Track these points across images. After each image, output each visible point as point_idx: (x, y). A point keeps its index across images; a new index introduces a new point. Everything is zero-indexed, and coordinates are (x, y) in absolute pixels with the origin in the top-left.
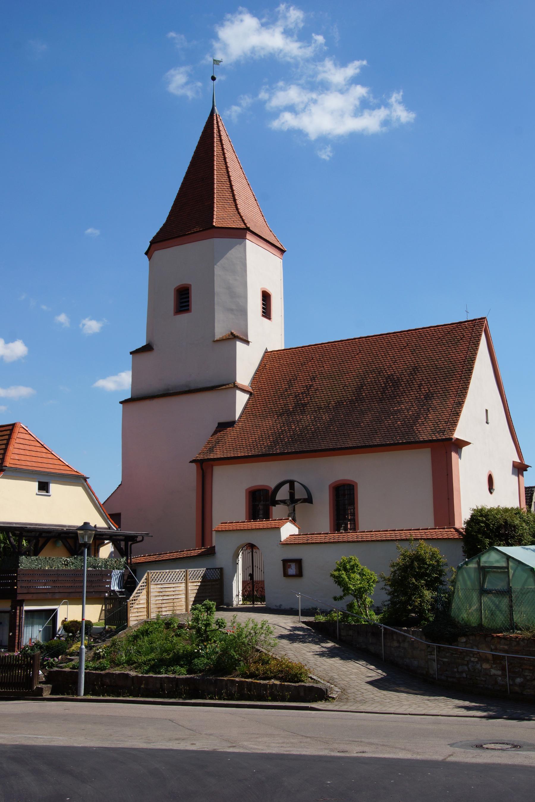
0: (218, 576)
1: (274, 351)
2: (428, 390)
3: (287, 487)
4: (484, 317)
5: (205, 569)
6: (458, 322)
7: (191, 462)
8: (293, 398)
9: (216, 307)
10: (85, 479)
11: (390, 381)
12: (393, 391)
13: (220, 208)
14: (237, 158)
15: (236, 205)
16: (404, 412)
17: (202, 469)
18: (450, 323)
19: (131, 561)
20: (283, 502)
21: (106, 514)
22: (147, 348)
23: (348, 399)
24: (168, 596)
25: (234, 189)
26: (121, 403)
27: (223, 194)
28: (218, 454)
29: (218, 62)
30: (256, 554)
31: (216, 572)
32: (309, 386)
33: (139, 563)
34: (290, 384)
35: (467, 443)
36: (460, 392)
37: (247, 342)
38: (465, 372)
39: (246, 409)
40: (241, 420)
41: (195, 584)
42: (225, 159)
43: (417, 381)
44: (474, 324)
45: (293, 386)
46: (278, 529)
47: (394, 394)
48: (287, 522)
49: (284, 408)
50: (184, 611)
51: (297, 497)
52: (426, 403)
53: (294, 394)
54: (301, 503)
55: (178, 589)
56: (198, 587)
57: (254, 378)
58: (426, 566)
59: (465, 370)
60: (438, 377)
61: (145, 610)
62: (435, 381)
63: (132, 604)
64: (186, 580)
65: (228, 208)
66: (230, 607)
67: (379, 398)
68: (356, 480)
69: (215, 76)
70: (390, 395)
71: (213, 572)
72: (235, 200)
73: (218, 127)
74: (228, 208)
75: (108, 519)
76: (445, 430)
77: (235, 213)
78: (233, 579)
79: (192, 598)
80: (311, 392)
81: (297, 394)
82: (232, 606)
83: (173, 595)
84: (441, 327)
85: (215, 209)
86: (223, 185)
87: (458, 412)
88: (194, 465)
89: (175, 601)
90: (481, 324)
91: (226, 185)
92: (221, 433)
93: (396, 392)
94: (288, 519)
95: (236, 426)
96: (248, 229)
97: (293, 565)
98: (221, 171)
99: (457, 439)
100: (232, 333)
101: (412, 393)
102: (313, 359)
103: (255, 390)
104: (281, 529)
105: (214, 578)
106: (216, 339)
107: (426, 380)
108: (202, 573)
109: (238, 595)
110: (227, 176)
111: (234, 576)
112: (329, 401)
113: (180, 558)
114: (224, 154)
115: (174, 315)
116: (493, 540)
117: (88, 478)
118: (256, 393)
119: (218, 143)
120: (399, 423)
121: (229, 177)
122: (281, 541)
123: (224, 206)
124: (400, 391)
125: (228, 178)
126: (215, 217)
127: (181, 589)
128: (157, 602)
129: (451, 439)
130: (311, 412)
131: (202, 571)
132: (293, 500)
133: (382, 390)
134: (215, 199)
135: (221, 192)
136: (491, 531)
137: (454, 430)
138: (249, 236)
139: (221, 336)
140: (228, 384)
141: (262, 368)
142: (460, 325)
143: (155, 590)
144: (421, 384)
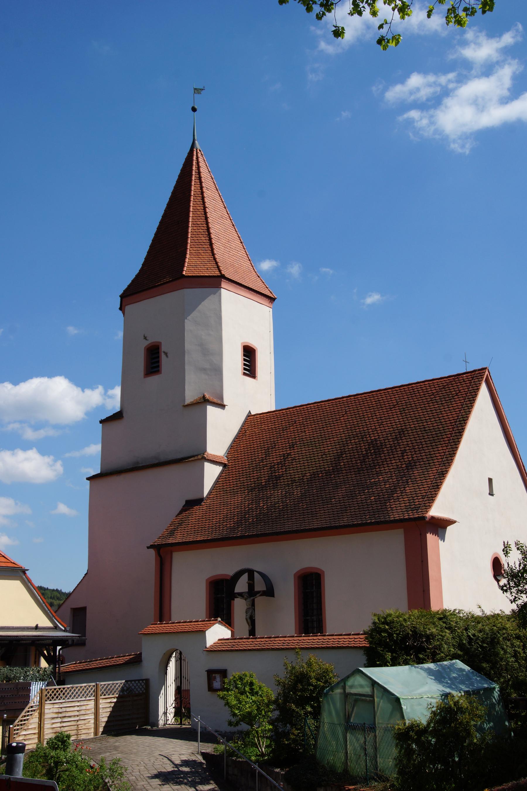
0: (143, 689)
1: (257, 414)
2: (412, 457)
3: (245, 577)
4: (485, 367)
5: (124, 681)
6: (456, 374)
7: (148, 548)
8: (268, 470)
9: (187, 367)
10: (24, 571)
11: (373, 447)
12: (374, 459)
13: (194, 254)
14: (220, 196)
15: (212, 250)
16: (381, 484)
17: (160, 556)
18: (447, 376)
19: (59, 670)
20: (241, 595)
21: (50, 612)
22: (117, 416)
23: (325, 470)
24: (70, 717)
25: (212, 231)
26: (88, 479)
27: (198, 238)
28: (178, 538)
29: (200, 91)
30: (184, 662)
31: (139, 684)
32: (286, 455)
33: (67, 672)
34: (267, 454)
35: (451, 522)
36: (446, 459)
37: (222, 406)
38: (455, 435)
39: (218, 483)
40: (211, 496)
41: (109, 701)
42: (203, 198)
43: (401, 447)
44: (473, 376)
45: (270, 455)
46: (203, 632)
47: (373, 463)
48: (214, 624)
49: (257, 482)
50: (92, 736)
51: (257, 589)
52: (407, 473)
53: (269, 465)
54: (260, 596)
55: (84, 708)
56: (113, 704)
57: (231, 447)
58: (311, 688)
59: (455, 433)
60: (425, 441)
61: (36, 736)
62: (421, 446)
63: (18, 730)
64: (96, 696)
65: (202, 254)
66: (155, 728)
67: (358, 468)
68: (323, 568)
69: (196, 107)
70: (369, 464)
71: (135, 685)
72: (211, 244)
73: (198, 163)
74: (202, 254)
75: (54, 617)
76: (420, 507)
77: (210, 259)
78: (160, 693)
79: (104, 718)
80: (287, 462)
81: (273, 464)
82: (158, 727)
83: (78, 716)
84: (437, 381)
85: (188, 256)
86: (198, 228)
87: (439, 484)
88: (152, 552)
89: (79, 723)
90: (481, 375)
91: (202, 228)
92: (186, 512)
93: (377, 460)
94: (217, 620)
95: (203, 504)
96: (223, 277)
97: (218, 677)
98: (198, 213)
99: (433, 518)
100: (204, 397)
101: (393, 462)
102: (295, 423)
103: (230, 461)
104: (207, 632)
105: (137, 692)
106: (186, 404)
107: (410, 445)
108: (119, 686)
109: (166, 713)
110: (204, 218)
111: (162, 689)
112: (304, 472)
113: (107, 666)
114: (202, 193)
115: (144, 377)
116: (397, 654)
117: (28, 570)
118: (231, 464)
119: (196, 181)
120: (373, 498)
121: (206, 218)
122: (206, 648)
123: (198, 252)
124: (381, 459)
125: (205, 219)
126: (186, 265)
127: (88, 707)
128: (54, 726)
129: (424, 518)
130: (284, 486)
131: (120, 683)
132: (251, 593)
133: (362, 458)
134: (189, 245)
135: (196, 236)
136: (395, 642)
137: (430, 507)
138: (224, 284)
139: (192, 400)
140: (197, 455)
141: (242, 434)
142: (457, 378)
143: (51, 711)
144: (405, 450)
